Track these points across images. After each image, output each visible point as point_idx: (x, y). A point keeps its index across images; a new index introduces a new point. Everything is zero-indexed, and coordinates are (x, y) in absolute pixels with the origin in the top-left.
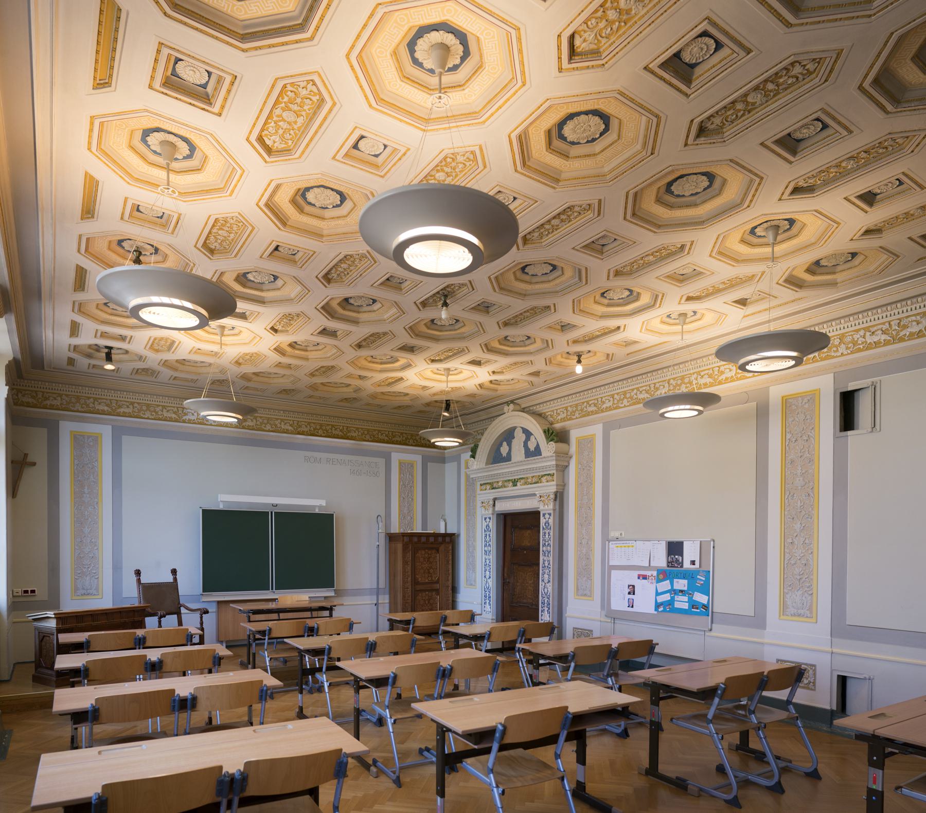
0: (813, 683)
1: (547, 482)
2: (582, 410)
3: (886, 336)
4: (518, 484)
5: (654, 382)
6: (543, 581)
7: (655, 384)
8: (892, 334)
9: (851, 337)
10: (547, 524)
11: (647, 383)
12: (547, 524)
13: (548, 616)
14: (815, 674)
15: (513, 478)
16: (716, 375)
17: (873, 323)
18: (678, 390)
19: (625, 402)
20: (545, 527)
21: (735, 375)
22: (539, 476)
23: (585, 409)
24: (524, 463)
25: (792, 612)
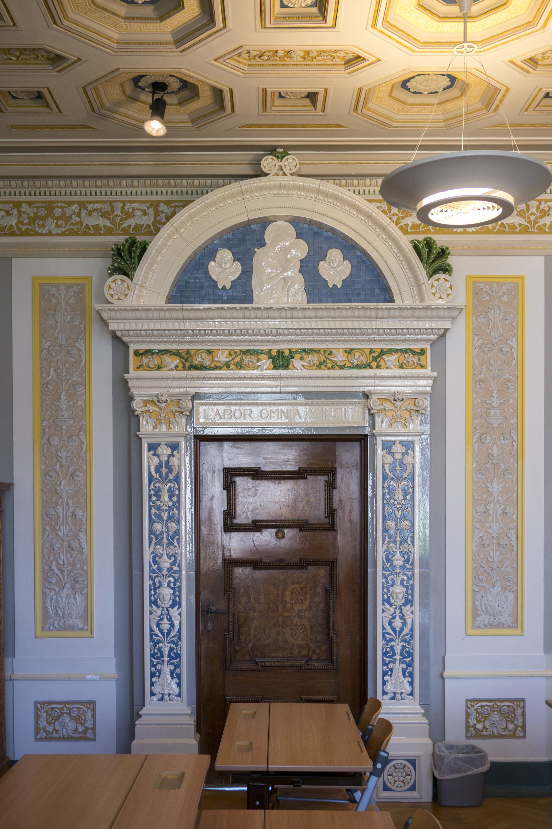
0: (92, 729)
1: (401, 367)
2: (63, 216)
3: (521, 219)
4: (296, 362)
5: (124, 198)
6: (387, 601)
7: (124, 203)
8: (529, 218)
9: (60, 210)
10: (164, 470)
11: (109, 198)
12: (164, 470)
13: (174, 686)
14: (523, 714)
15: (275, 347)
16: (533, 214)
17: (93, 198)
18: (40, 226)
19: (51, 224)
20: (156, 476)
21: (17, 224)
22: (371, 351)
23: (76, 219)
24: (162, 314)
25: (486, 622)
